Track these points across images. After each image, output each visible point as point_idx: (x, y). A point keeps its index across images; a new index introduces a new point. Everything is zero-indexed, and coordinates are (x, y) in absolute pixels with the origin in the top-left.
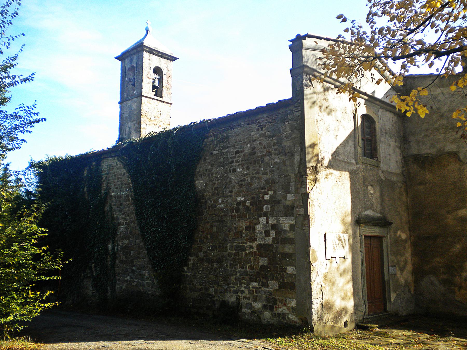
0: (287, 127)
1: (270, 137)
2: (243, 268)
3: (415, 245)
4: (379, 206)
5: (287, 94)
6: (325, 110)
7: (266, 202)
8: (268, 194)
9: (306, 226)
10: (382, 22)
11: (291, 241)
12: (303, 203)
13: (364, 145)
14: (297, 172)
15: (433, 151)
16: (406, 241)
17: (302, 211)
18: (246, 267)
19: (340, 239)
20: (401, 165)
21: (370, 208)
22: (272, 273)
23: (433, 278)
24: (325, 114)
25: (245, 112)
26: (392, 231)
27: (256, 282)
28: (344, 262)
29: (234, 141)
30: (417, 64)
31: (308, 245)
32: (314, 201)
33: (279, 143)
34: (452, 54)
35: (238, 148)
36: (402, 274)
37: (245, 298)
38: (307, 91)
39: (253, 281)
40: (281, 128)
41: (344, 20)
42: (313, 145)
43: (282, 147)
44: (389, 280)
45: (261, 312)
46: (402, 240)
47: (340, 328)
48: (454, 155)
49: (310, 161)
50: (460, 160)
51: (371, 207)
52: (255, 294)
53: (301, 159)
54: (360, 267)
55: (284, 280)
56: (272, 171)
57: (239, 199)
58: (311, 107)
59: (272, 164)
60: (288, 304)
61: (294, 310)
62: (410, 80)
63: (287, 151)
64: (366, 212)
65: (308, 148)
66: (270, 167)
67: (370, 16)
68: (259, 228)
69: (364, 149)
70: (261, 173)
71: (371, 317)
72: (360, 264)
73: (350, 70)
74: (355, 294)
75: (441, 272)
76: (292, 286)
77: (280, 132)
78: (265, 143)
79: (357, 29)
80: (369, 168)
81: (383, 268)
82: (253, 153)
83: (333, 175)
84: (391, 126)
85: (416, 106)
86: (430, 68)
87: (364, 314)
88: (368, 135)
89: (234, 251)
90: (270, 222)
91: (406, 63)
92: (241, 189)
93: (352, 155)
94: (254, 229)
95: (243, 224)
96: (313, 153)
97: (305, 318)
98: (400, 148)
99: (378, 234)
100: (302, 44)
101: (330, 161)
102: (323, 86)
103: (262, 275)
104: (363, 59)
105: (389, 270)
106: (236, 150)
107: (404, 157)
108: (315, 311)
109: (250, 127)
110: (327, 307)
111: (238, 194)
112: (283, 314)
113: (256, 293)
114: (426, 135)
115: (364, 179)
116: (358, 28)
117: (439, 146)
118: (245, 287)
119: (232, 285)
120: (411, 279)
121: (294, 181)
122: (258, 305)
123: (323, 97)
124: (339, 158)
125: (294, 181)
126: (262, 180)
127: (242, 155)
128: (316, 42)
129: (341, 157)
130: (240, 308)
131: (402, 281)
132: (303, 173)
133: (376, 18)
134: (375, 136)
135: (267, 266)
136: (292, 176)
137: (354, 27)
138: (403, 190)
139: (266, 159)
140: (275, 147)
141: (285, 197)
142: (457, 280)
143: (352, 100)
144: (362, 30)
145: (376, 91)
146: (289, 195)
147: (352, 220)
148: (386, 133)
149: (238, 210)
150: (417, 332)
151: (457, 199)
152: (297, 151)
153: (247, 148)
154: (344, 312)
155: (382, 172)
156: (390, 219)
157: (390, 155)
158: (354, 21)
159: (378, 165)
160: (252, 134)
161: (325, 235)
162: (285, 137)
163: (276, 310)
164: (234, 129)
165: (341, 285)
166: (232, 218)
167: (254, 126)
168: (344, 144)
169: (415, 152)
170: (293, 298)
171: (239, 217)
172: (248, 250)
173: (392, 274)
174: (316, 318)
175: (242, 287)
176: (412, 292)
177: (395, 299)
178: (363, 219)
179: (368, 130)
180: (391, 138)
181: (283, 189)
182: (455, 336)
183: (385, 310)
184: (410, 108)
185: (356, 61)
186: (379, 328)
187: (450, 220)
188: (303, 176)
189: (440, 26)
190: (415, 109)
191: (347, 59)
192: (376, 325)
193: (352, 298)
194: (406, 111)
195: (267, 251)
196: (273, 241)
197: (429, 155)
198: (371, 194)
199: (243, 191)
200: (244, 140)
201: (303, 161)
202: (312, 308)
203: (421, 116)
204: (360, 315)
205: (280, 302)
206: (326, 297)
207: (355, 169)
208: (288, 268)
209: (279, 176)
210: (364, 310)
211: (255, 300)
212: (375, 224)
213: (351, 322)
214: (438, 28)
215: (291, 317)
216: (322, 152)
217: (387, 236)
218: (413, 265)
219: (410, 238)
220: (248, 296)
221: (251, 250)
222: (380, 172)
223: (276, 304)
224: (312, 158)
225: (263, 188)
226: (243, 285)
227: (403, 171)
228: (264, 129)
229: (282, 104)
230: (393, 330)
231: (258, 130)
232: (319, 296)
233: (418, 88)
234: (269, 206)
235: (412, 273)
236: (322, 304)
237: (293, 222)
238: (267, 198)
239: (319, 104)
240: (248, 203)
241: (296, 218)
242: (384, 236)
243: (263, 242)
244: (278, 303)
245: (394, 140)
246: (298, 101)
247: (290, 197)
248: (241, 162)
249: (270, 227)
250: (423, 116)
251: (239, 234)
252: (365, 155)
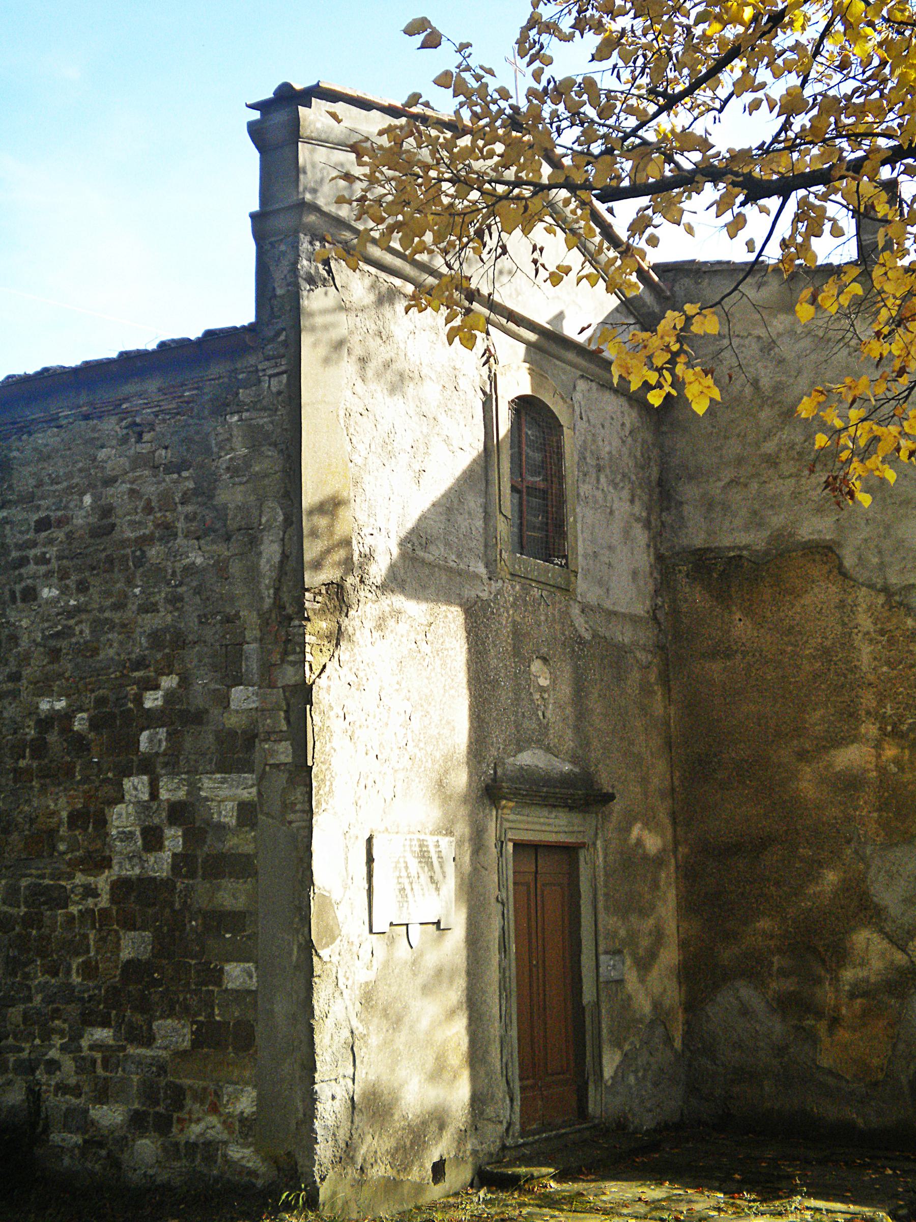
0: (235, 432)
1: (170, 468)
2: (55, 974)
3: (689, 874)
4: (569, 734)
5: (242, 313)
6: (378, 375)
7: (151, 719)
8: (157, 687)
9: (298, 807)
10: (572, 58)
11: (242, 866)
12: (288, 720)
13: (521, 511)
14: (268, 602)
15: (756, 540)
16: (658, 861)
17: (284, 752)
18: (68, 972)
19: (424, 857)
20: (651, 587)
21: (538, 741)
22: (167, 989)
23: (746, 992)
24: (378, 389)
25: (75, 371)
26: (611, 827)
27: (105, 1024)
28: (440, 939)
29: (32, 482)
30: (686, 218)
31: (307, 879)
32: (332, 714)
33: (204, 492)
34: (802, 192)
35: (46, 508)
36: (642, 981)
37: (63, 1088)
38: (315, 301)
39: (93, 1025)
40: (213, 436)
41: (432, 41)
42: (332, 506)
43: (214, 508)
44: (597, 1004)
45: (123, 1143)
46: (645, 857)
47: (419, 1188)
48: (825, 551)
49: (317, 565)
50: (844, 574)
51: (539, 740)
52: (100, 1071)
53: (285, 556)
54: (495, 958)
55: (212, 1014)
56: (175, 600)
57: (44, 706)
58: (327, 361)
59: (174, 572)
60: (225, 1106)
61: (246, 1127)
62: (687, 282)
63: (232, 525)
64: (519, 756)
65: (311, 513)
66: (169, 584)
67: (533, 33)
68: (122, 818)
69: (521, 524)
70: (133, 607)
71: (531, 1139)
72: (495, 946)
73: (460, 228)
74: (476, 1056)
75: (775, 968)
76: (244, 1038)
77: (208, 451)
78: (150, 490)
79: (478, 78)
80: (536, 593)
81: (579, 961)
82: (104, 528)
83: (403, 617)
84: (616, 443)
85: (680, 369)
86: (732, 236)
87: (507, 1130)
88: (535, 473)
89: (23, 910)
90: (164, 795)
91: (649, 212)
92: (56, 666)
93: (477, 544)
94: (102, 822)
95: (60, 805)
96: (332, 534)
97: (289, 1154)
98: (647, 525)
99: (562, 838)
100: (296, 121)
101: (392, 567)
102: (373, 286)
103: (133, 997)
104: (501, 189)
105: (598, 966)
106: (36, 517)
107: (660, 558)
108: (326, 1127)
109: (94, 430)
110: (371, 1107)
111: (44, 688)
112: (208, 1144)
113: (105, 1067)
114: (734, 482)
115: (517, 634)
116: (482, 73)
117: (777, 520)
118: (63, 1048)
119: (11, 1040)
120: (673, 995)
121: (255, 640)
122: (110, 1116)
123: (373, 328)
124: (429, 558)
125: (255, 640)
126: (136, 635)
127: (60, 535)
128: (334, 116)
129: (435, 553)
130: (40, 1129)
131: (643, 1005)
132: (290, 610)
133: (552, 45)
134: (561, 478)
135: (148, 962)
136: (250, 618)
137: (468, 69)
138: (653, 678)
139: (154, 552)
140: (189, 508)
141: (224, 701)
142: (826, 995)
143: (457, 339)
144: (493, 84)
145: (566, 313)
146: (238, 694)
147: (470, 784)
148: (599, 469)
149: (39, 748)
150: (685, 1186)
151: (832, 711)
152: (269, 527)
153: (81, 508)
154: (433, 1127)
155: (583, 611)
156: (605, 781)
157: (610, 548)
158: (469, 45)
159: (569, 583)
160: (102, 454)
161: (370, 841)
162: (228, 468)
163: (182, 1130)
164: (30, 434)
165: (424, 1024)
166: (15, 781)
167: (111, 426)
168: (449, 505)
169: (699, 541)
170: (247, 1084)
171: (44, 777)
172: (78, 903)
173: (607, 982)
174: (329, 1154)
175: (51, 1046)
176: (678, 1044)
177: (616, 1073)
178: (511, 780)
179: (538, 456)
180: (616, 486)
181: (215, 667)
182: (809, 1195)
183: (582, 1111)
184: (661, 375)
185: (475, 195)
186: (560, 1177)
187: (807, 784)
188: (290, 619)
189: (767, 90)
190: (677, 383)
191: (445, 186)
192: (545, 1170)
193: (465, 1075)
194: (647, 387)
195: (154, 904)
196: (175, 867)
197: (745, 553)
198: (542, 689)
199: (60, 675)
200: (69, 476)
201: (292, 564)
202: (313, 1116)
203: (694, 407)
204: (493, 1132)
205: (195, 1098)
206: (368, 1073)
207: (484, 596)
208: (227, 967)
209: (203, 620)
210: (505, 1114)
211: (102, 1096)
212: (551, 801)
213: (459, 1160)
214: (760, 95)
215: (236, 1153)
216: (366, 531)
217: (594, 844)
218: (683, 945)
219: (675, 850)
220: (72, 1081)
221: (90, 901)
222: (575, 610)
223: (181, 1107)
224: (328, 551)
225: (140, 664)
226: (58, 1041)
227: (655, 608)
228: (147, 437)
229: (218, 343)
230: (602, 1185)
231: (124, 440)
232: (341, 1071)
233: (687, 307)
234: (162, 733)
235: (678, 977)
236: (352, 1099)
237: (248, 794)
238: (152, 700)
239: (358, 351)
240: (80, 723)
241: (261, 778)
242: (583, 845)
243: (137, 871)
244: (188, 1102)
245: (626, 494)
246: (278, 334)
247: (242, 697)
248: (54, 564)
249: (164, 815)
250: (700, 407)
251: (43, 840)
252: (521, 546)
